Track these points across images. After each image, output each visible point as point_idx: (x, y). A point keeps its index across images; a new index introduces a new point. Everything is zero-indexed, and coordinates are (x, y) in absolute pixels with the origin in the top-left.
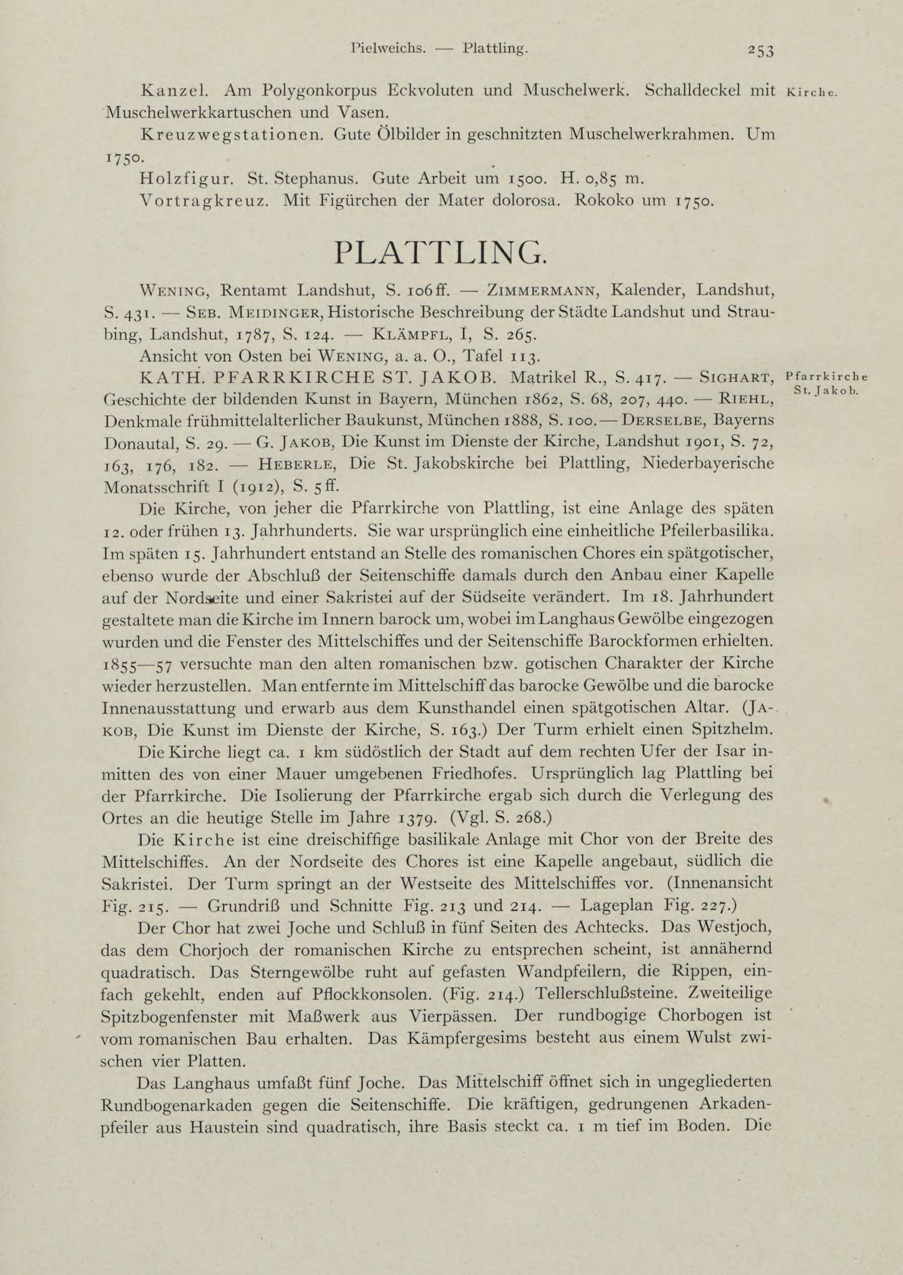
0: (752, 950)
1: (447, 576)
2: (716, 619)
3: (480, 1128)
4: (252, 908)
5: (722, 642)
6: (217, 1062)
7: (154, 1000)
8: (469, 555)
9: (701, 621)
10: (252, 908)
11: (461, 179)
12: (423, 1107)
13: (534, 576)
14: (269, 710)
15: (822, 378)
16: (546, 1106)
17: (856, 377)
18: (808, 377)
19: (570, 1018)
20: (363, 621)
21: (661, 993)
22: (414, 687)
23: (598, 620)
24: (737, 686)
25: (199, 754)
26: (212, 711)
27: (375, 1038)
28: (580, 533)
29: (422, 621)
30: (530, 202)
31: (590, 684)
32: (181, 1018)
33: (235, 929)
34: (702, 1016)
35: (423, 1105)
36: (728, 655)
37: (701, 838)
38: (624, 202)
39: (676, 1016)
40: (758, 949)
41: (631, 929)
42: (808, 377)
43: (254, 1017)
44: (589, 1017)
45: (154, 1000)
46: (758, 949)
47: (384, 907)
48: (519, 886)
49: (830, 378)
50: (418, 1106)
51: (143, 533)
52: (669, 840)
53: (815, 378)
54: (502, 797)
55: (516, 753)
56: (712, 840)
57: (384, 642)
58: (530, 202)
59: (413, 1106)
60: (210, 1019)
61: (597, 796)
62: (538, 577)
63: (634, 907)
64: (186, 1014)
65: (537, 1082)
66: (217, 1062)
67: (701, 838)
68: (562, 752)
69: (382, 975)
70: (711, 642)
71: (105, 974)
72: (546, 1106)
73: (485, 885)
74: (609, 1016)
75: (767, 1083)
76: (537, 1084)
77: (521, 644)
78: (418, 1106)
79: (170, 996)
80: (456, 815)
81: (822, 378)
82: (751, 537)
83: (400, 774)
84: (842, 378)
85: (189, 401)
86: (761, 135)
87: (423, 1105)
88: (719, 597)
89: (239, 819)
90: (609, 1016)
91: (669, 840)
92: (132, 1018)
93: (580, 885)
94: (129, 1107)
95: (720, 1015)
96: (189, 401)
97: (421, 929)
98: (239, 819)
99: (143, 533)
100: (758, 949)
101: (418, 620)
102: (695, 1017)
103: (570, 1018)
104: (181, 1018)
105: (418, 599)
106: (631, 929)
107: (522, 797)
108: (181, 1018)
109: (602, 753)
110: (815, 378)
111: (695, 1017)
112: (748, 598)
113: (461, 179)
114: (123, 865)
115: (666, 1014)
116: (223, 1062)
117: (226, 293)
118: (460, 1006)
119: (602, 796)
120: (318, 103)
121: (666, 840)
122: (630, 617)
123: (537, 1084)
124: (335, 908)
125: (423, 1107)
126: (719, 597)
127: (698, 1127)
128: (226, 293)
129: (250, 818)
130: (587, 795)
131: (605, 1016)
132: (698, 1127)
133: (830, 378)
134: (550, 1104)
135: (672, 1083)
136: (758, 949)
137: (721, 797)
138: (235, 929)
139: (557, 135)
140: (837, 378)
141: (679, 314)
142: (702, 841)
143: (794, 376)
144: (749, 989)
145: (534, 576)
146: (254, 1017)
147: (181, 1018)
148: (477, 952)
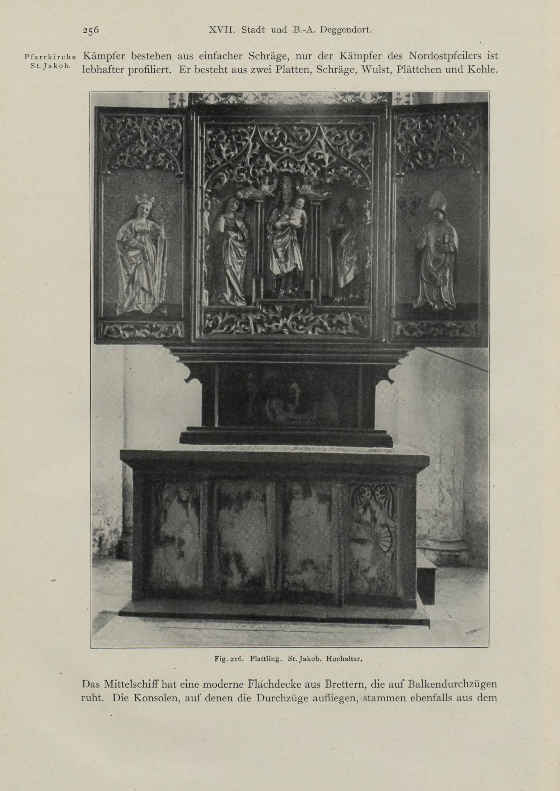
0: (232, 685)
2: (346, 70)
4: (444, 685)
6: (294, 70)
8: (205, 71)
9: (188, 686)
10: (444, 685)
12: (148, 686)
13: (447, 684)
17: (68, 57)
18: (39, 58)
20: (357, 685)
21: (191, 685)
22: (114, 685)
28: (188, 686)
29: (290, 685)
30: (137, 70)
32: (430, 698)
33: (173, 685)
35: (148, 684)
36: (471, 65)
38: (296, 686)
40: (236, 685)
41: (293, 686)
42: (39, 58)
43: (206, 685)
46: (236, 685)
48: (107, 686)
50: (145, 685)
51: (220, 685)
55: (237, 70)
56: (336, 685)
58: (137, 70)
59: (463, 685)
61: (454, 685)
62: (451, 686)
64: (432, 696)
65: (155, 684)
66: (294, 70)
70: (229, 685)
75: (494, 685)
76: (155, 686)
77: (351, 686)
78: (145, 685)
79: (429, 685)
82: (424, 688)
83: (438, 685)
87: (148, 684)
93: (145, 685)
99: (220, 685)
100: (236, 685)
104: (430, 699)
106: (293, 686)
108: (430, 698)
110: (43, 58)
114: (117, 686)
116: (124, 685)
119: (457, 685)
123: (155, 686)
125: (148, 686)
127: (217, 685)
129: (483, 684)
132: (217, 685)
134: (483, 684)
136: (236, 685)
138: (173, 685)
139: (494, 684)
142: (329, 686)
145: (447, 684)
146: (206, 685)
147: (430, 699)
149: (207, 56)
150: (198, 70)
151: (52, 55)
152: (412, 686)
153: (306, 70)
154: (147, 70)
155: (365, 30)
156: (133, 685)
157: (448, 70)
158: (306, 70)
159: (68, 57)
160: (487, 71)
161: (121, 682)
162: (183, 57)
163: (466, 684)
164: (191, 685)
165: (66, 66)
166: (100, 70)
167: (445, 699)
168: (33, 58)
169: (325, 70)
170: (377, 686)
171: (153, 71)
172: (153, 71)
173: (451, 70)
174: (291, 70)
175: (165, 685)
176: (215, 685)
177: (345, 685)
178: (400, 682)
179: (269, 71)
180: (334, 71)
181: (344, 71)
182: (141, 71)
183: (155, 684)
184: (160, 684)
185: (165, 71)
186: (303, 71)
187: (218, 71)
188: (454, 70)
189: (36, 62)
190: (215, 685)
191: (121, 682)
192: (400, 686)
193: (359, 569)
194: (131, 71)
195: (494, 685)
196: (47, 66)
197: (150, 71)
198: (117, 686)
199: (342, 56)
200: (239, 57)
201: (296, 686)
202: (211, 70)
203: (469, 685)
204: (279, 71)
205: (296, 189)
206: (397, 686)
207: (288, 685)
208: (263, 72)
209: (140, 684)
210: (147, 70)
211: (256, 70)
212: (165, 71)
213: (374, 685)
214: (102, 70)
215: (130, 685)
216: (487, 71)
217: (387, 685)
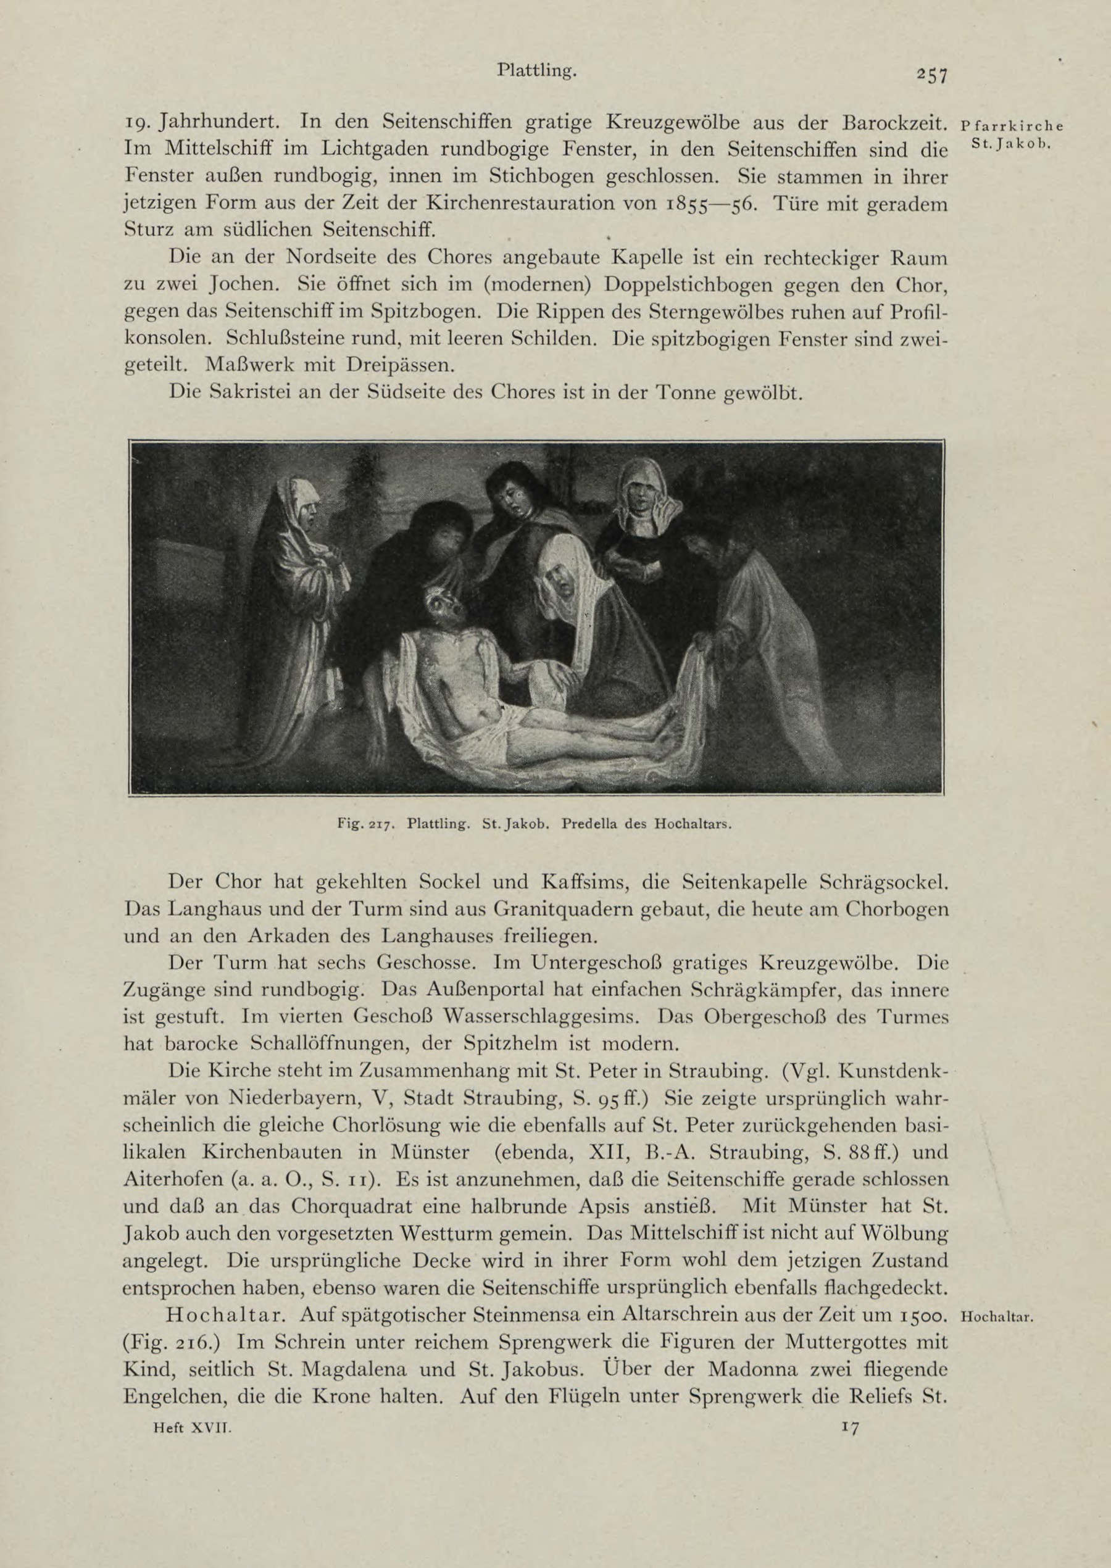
1: (489, 122)
5: (207, 122)
7: (711, 319)
8: (475, 394)
9: (438, 1209)
12: (252, 151)
14: (298, 911)
15: (1007, 128)
16: (570, 125)
19: (276, 992)
23: (863, 314)
24: (874, 125)
25: (463, 204)
26: (495, 1182)
27: (390, 989)
30: (179, 1289)
34: (899, 911)
35: (253, 149)
38: (227, 1046)
39: (867, 910)
40: (557, 285)
41: (902, 126)
42: (991, 128)
44: (479, 151)
45: (711, 319)
46: (557, 286)
49: (1018, 127)
51: (637, 1045)
53: (999, 128)
54: (306, 1235)
55: (863, 314)
57: (465, 122)
58: (179, 1289)
59: (240, 150)
60: (436, 1155)
61: (704, 1343)
63: (547, 1018)
68: (527, 1234)
71: (174, 1235)
72: (570, 125)
73: (393, 204)
74: (336, 177)
78: (810, 151)
79: (459, 1263)
81: (1007, 128)
83: (539, 1153)
88: (207, 122)
89: (563, 123)
90: (503, 151)
92: (502, 1045)
93: (810, 151)
95: (566, 176)
96: (484, 1127)
97: (618, 1181)
98: (563, 123)
99: (637, 1045)
100: (557, 286)
101: (893, 124)
102: (891, 911)
103: (366, 341)
106: (902, 126)
107: (265, 1290)
109: (459, 123)
110: (999, 128)
111: (891, 911)
112: (242, 123)
114: (657, 1236)
115: (301, 1205)
120: (893, 138)
121: (803, 125)
125: (471, 125)
126: (207, 122)
127: (631, 1046)
130: (799, 993)
131: (318, 991)
132: (631, 1046)
134: (576, 122)
135: (365, 1045)
136: (557, 285)
139: (363, 122)
140: (1025, 128)
141: (697, 912)
148: (139, 286)
152: (850, 126)
153: (399, 1045)
154: (929, 313)
155: (266, 123)
156: (687, 1235)
161: (198, 143)
163: (279, 1044)
164: (153, 1371)
167: (803, 1291)
170: (634, 1344)
175: (887, 1207)
176: (515, 286)
177: (881, 1343)
179: (846, 1372)
183: (265, 149)
184: (739, 1233)
190: (515, 286)
191: (198, 143)
192: (848, 1236)
193: (493, 726)
195: (940, 259)
198: (657, 1236)
201: (464, 885)
203: (479, 1182)
205: (421, 594)
206: (198, 1019)
207: (445, 1263)
209: (235, 148)
210: (929, 313)
213: (723, 911)
215: (666, 286)
217: (806, 910)
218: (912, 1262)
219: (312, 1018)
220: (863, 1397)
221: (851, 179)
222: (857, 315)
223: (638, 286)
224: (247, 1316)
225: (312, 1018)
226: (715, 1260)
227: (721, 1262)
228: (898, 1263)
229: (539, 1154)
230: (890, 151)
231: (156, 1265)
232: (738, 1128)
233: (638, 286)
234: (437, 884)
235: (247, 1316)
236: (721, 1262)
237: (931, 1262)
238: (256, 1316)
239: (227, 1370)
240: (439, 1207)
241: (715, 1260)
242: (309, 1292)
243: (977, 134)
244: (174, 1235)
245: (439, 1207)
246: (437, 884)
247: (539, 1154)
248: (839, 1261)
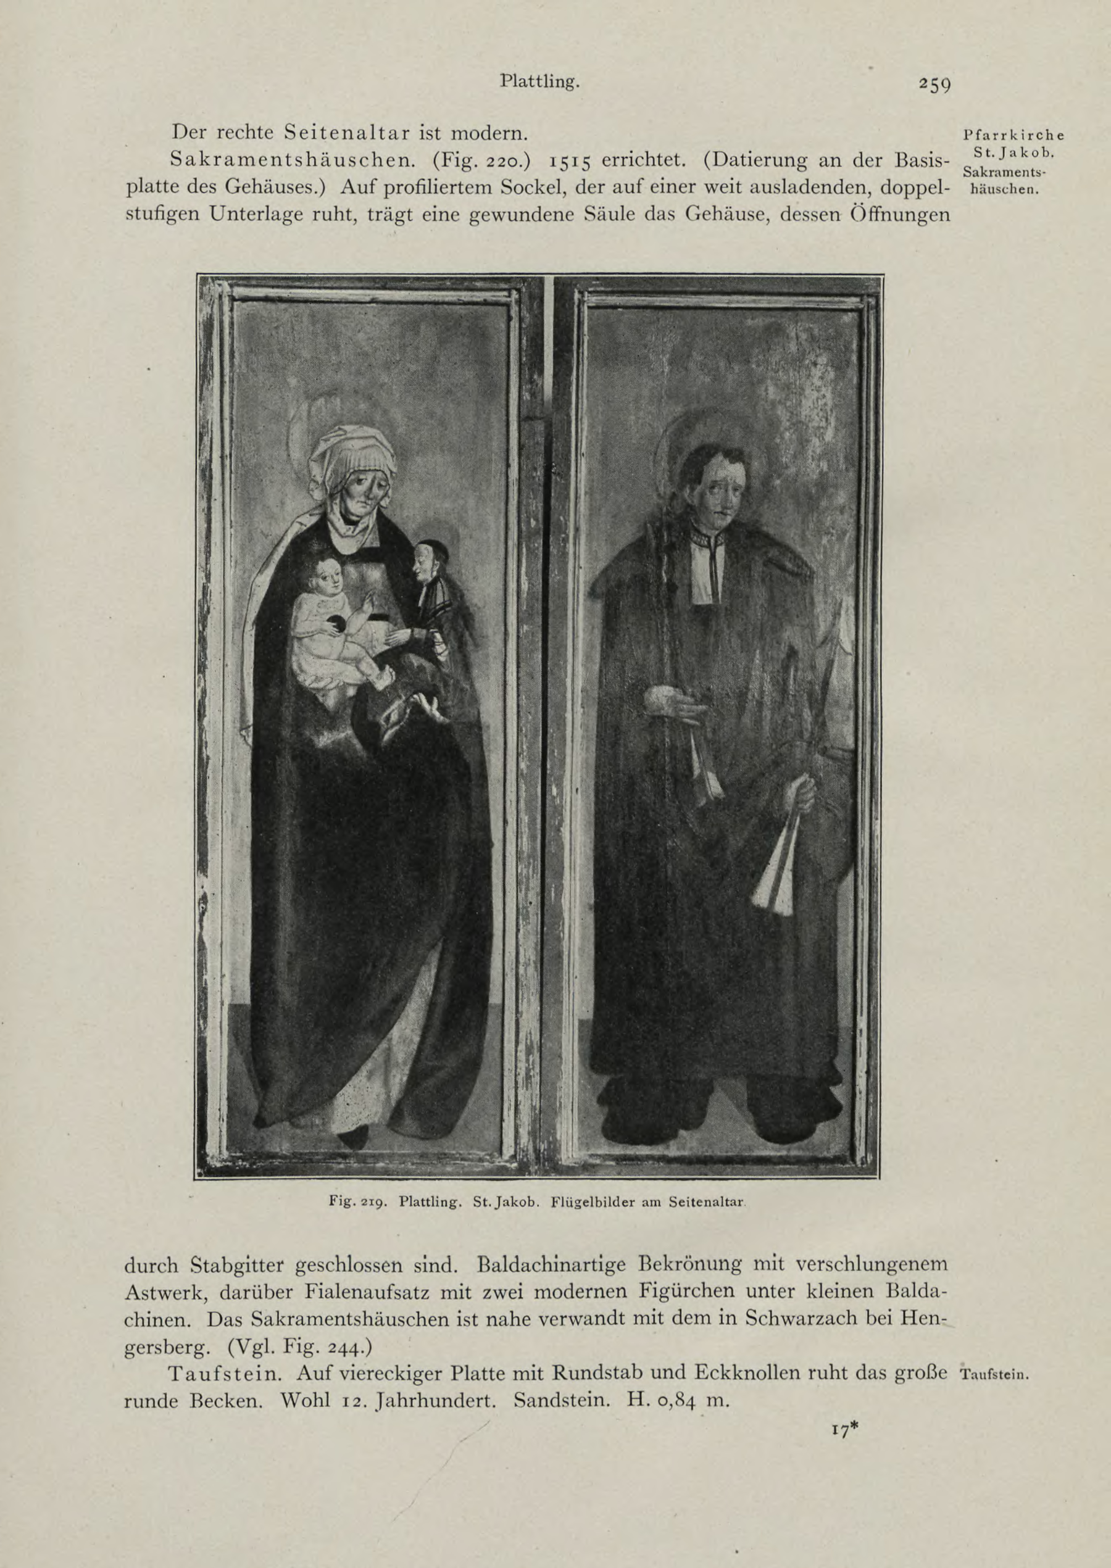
2: (922, 215)
3: (934, 162)
6: (161, 187)
8: (209, 188)
11: (735, 187)
15: (1008, 137)
17: (1049, 137)
18: (992, 137)
23: (623, 188)
27: (216, 1319)
30: (402, 189)
31: (233, 185)
37: (902, 160)
41: (538, 190)
42: (992, 137)
47: (168, 187)
49: (1019, 137)
52: (862, 161)
53: (999, 137)
54: (192, 1349)
58: (402, 189)
63: (144, 188)
66: (161, 187)
67: (902, 160)
69: (829, 1376)
71: (638, 1374)
73: (192, 188)
80: (235, 1344)
81: (1008, 137)
84: (1034, 137)
85: (183, 189)
86: (227, 215)
91: (862, 161)
94: (525, 216)
96: (183, 189)
101: (530, 189)
105: (369, 190)
106: (538, 190)
112: (838, 189)
113: (735, 187)
117: (559, 1376)
118: (451, 174)
122: (241, 185)
124: (507, 190)
128: (559, 1376)
133: (1019, 137)
137: (784, 163)
140: (1026, 137)
143: (974, 135)
144: (433, 182)
149: (438, 215)
150: (872, 1319)
151: (1017, 132)
152: (197, 1404)
153: (861, 189)
154: (421, 188)
157: (731, 1319)
158: (861, 189)
159: (1049, 137)
160: (347, 1268)
162: (623, 188)
165: (1045, 153)
166: (368, 1321)
168: (981, 136)
169: (763, 1320)
171: (433, 190)
172: (433, 190)
173: (145, 1402)
174: (155, 187)
178: (635, 182)
179: (518, 1295)
180: (409, 1403)
181: (394, 216)
182: (409, 189)
185: (483, 1402)
186: (334, 1321)
187: (252, 189)
188: (586, 1374)
189: (984, 145)
194: (390, 189)
196: (1007, 153)
197: (427, 190)
199: (558, 1373)
200: (597, 189)
202: (524, 216)
204: (457, 1376)
208: (507, 1296)
210: (421, 188)
211: (492, 1293)
212: (483, 1402)
214: (571, 1267)
216: (347, 1268)
218: (619, 1374)
219: (456, 189)
220: (566, 1374)
221: (821, 189)
222: (617, 189)
223: (910, 189)
224: (377, 134)
225: (456, 189)
226: (319, 1401)
227: (325, 1403)
228: (397, 1322)
229: (827, 189)
230: (672, 187)
231: (423, 1377)
232: (608, 189)
233: (910, 189)
234: (519, 189)
235: (377, 134)
236: (325, 1403)
237: (543, 1402)
238: (386, 134)
239: (433, 187)
240: (666, 187)
241: (319, 1401)
242: (876, 192)
243: (1004, 143)
244: (638, 1374)
245: (666, 187)
246: (519, 189)
247: (827, 189)
248: (135, 1347)
